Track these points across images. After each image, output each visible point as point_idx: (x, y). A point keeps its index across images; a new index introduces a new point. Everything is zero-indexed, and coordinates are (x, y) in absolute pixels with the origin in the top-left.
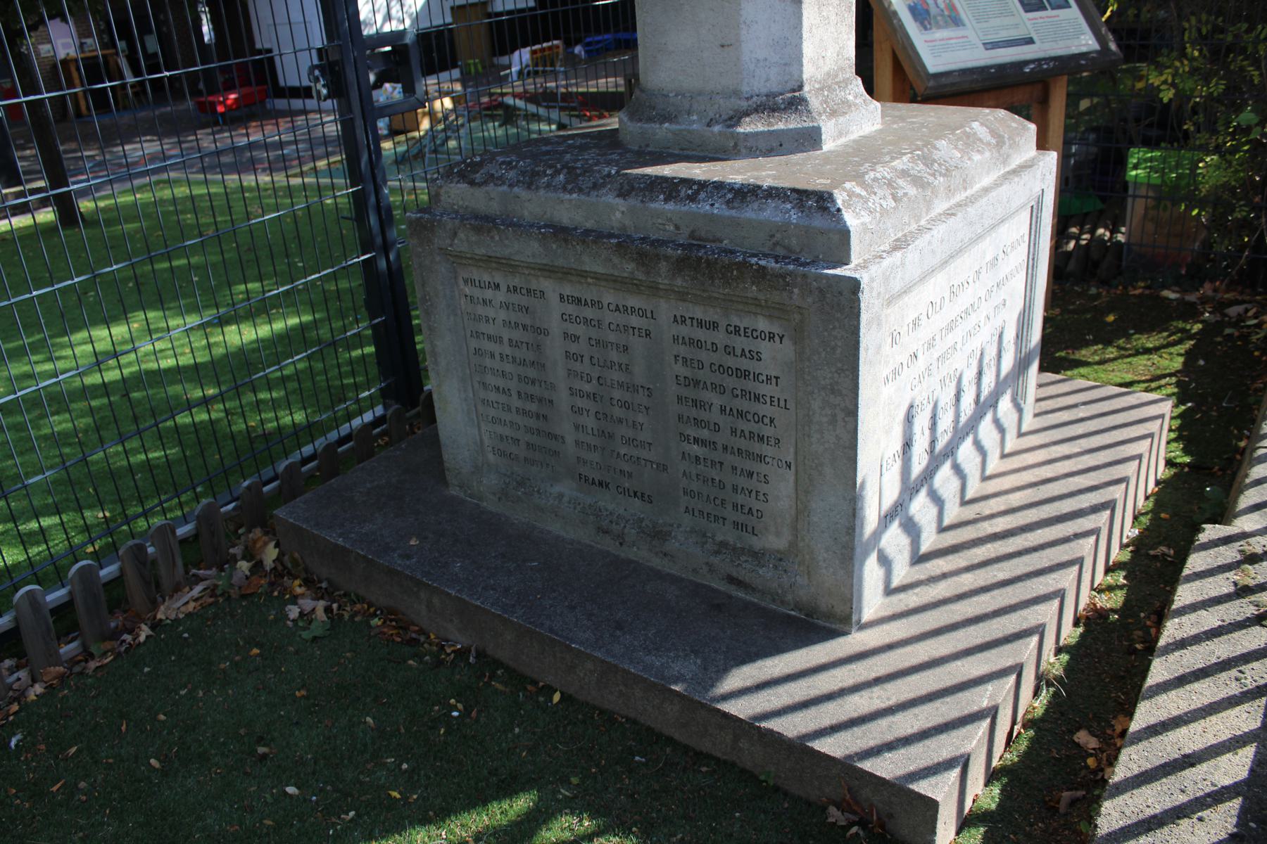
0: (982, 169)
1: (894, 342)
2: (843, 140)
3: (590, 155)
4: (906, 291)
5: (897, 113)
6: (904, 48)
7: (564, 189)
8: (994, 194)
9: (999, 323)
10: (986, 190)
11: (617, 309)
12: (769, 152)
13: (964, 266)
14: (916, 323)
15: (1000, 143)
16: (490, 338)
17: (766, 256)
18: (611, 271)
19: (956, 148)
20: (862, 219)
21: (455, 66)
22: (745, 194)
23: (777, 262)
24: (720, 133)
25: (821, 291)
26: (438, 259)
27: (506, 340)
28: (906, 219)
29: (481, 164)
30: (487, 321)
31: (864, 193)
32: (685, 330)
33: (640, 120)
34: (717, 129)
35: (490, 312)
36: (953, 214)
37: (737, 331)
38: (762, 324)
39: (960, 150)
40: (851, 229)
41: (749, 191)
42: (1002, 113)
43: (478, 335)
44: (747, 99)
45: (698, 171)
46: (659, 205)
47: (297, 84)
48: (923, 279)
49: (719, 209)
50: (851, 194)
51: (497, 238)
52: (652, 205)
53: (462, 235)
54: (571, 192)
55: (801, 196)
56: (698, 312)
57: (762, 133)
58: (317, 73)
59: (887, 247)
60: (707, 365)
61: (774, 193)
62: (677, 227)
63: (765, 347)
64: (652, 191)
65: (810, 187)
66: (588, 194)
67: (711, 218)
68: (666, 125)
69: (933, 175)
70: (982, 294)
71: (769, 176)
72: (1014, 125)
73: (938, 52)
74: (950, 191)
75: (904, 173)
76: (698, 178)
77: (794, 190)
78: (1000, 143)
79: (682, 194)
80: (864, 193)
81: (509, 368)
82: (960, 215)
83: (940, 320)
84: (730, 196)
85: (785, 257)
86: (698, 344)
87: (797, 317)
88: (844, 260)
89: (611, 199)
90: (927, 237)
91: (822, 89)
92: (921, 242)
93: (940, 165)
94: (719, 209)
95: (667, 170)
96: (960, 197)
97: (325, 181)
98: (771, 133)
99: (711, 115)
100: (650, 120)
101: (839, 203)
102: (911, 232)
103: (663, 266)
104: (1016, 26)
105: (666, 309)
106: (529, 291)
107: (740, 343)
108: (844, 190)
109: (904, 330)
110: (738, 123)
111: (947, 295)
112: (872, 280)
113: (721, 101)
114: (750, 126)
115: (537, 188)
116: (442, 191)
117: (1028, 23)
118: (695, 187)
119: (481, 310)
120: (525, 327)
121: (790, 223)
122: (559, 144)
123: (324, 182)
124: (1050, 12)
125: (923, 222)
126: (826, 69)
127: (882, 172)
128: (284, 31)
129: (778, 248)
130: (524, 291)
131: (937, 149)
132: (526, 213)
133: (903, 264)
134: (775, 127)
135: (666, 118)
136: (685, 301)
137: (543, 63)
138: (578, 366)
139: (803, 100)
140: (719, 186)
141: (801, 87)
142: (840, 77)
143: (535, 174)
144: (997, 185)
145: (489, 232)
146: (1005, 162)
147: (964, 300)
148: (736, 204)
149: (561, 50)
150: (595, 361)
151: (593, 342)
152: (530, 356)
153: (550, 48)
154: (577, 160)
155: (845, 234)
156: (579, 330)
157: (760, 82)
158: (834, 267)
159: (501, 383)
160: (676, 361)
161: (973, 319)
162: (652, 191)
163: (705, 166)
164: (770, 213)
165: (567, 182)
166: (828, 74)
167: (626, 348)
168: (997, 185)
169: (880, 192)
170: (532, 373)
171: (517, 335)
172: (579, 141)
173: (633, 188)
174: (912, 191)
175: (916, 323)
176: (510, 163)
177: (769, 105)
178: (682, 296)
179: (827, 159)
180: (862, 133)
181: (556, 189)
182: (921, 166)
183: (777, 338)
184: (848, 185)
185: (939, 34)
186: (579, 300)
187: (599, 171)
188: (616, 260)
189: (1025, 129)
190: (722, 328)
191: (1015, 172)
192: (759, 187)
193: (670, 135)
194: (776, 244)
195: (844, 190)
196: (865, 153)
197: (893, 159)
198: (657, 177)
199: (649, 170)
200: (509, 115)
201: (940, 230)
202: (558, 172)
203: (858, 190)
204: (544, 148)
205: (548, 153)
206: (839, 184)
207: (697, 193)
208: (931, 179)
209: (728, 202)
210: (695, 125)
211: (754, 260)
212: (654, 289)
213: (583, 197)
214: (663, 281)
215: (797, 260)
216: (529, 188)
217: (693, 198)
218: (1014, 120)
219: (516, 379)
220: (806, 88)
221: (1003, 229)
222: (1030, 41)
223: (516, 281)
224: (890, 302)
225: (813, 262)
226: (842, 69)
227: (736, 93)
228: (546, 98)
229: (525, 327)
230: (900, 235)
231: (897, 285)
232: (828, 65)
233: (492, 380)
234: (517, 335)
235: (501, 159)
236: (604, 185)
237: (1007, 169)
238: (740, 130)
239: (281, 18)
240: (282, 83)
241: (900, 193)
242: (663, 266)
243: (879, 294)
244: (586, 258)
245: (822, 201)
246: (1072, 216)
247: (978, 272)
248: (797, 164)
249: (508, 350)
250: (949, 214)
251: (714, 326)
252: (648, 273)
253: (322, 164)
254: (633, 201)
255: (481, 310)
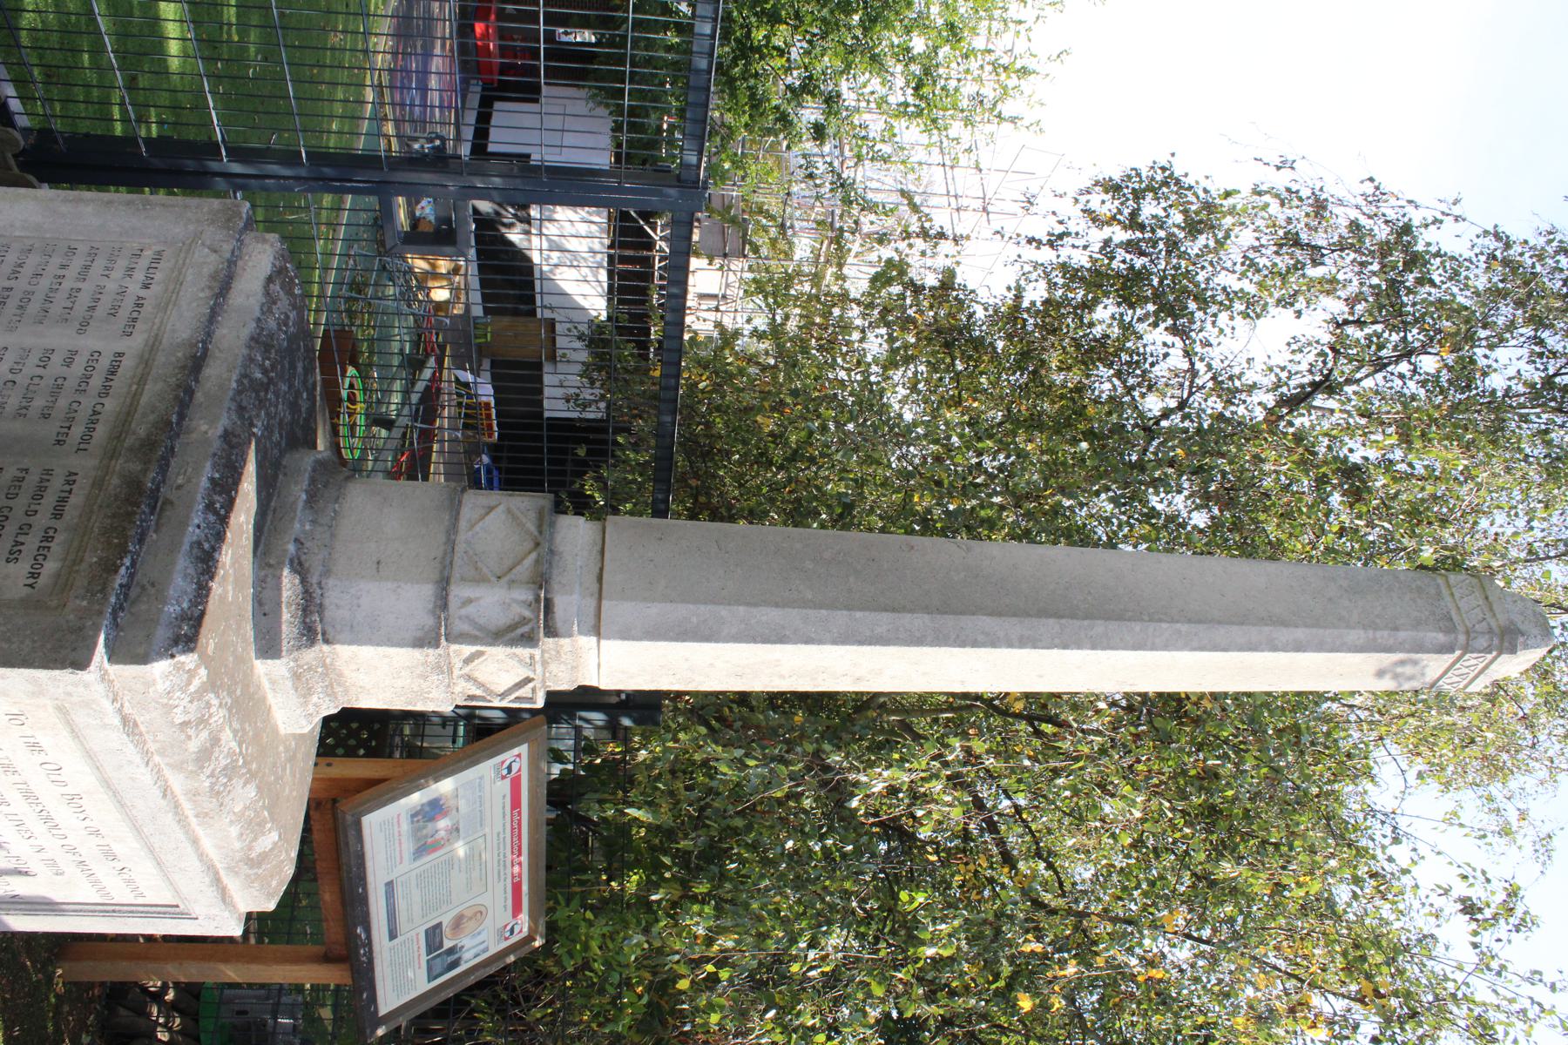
0: (221, 838)
1: (14, 716)
2: (266, 685)
3: (282, 410)
4: (75, 733)
5: (300, 756)
6: (393, 790)
7: (245, 376)
8: (189, 849)
9: (34, 865)
10: (195, 842)
11: (95, 413)
12: (258, 601)
13: (103, 812)
14: (35, 747)
15: (253, 863)
16: (87, 267)
17: (132, 576)
18: (140, 410)
19: (246, 808)
20: (160, 681)
21: (487, 311)
22: (206, 562)
23: (121, 586)
24: (286, 551)
25: (80, 629)
26: (191, 227)
27: (80, 285)
28: (160, 737)
29: (290, 293)
30: (107, 269)
31: (192, 688)
32: (57, 483)
33: (314, 470)
34: (291, 548)
35: (117, 274)
36: (165, 796)
37: (48, 539)
38: (50, 567)
39: (242, 813)
40: (148, 667)
41: (209, 567)
42: (289, 871)
43: (93, 254)
44: (319, 583)
45: (242, 518)
46: (207, 471)
47: (493, 122)
48: (89, 755)
49: (192, 533)
50: (191, 674)
51: (201, 295)
52: (208, 465)
53: (213, 257)
54: (239, 382)
55: (197, 621)
56: (76, 500)
57: (280, 595)
58: (438, 143)
59: (127, 709)
60: (11, 503)
61: (202, 592)
62: (179, 487)
63: (23, 567)
64: (226, 466)
65: (204, 631)
66: (232, 399)
67: (184, 524)
68: (304, 496)
69: (212, 775)
70: (71, 841)
71: (225, 592)
72: (274, 883)
73: (385, 831)
74: (194, 794)
75: (215, 741)
76: (233, 516)
77: (203, 613)
78: (253, 863)
79: (216, 497)
80: (192, 688)
81: (45, 283)
82: (164, 803)
83: (40, 783)
84: (206, 546)
85: (126, 596)
86: (38, 495)
87: (54, 603)
88: (114, 656)
89: (223, 422)
90: (137, 759)
91: (324, 665)
92: (131, 751)
93: (225, 785)
94: (192, 533)
95: (248, 487)
96: (187, 807)
97: (365, 126)
98: (279, 604)
99: (308, 544)
100: (313, 481)
101: (181, 658)
102: (145, 742)
103: (136, 467)
104: (410, 920)
105: (85, 466)
106: (135, 320)
107: (32, 542)
108: (198, 667)
109: (27, 730)
110: (294, 570)
111: (69, 790)
112: (86, 686)
113: (320, 557)
114: (289, 583)
115: (250, 347)
116: (267, 247)
117: (413, 933)
118: (222, 512)
119: (122, 263)
120: (92, 308)
121: (165, 603)
122: (305, 382)
123: (369, 122)
124: (424, 958)
125: (157, 759)
126: (346, 673)
127: (218, 716)
128: (556, 122)
129: (138, 590)
130: (135, 315)
131: (245, 785)
132: (225, 331)
133: (105, 726)
134: (284, 610)
135: (312, 498)
136: (93, 485)
137: (471, 416)
138: (33, 359)
139: (312, 642)
140: (220, 537)
141: (327, 641)
142: (338, 689)
143: (267, 348)
144: (201, 856)
145: (210, 288)
146: (229, 869)
147: (64, 815)
148: (195, 550)
149: (486, 439)
150: (36, 380)
151: (60, 382)
152: (56, 309)
153: (490, 427)
154: (277, 394)
155: (143, 659)
156: (78, 368)
157: (338, 599)
158: (106, 645)
159: (28, 270)
160: (22, 470)
161: (39, 828)
162: (226, 466)
163: (249, 528)
164: (180, 583)
165: (251, 380)
166: (341, 675)
167: (45, 416)
168: (201, 856)
169: (193, 707)
170: (34, 307)
171: (84, 300)
172: (304, 406)
173: (232, 447)
174: (193, 746)
175: (35, 747)
176: (286, 325)
177: (310, 606)
178: (99, 483)
179: (241, 660)
180: (274, 708)
181: (245, 366)
182: (224, 762)
183: (31, 581)
184: (203, 672)
185: (405, 826)
186: (113, 373)
187: (258, 416)
188: (152, 417)
189: (270, 896)
190: (53, 523)
191: (217, 881)
192: (212, 578)
193: (292, 499)
194: (143, 588)
195: (198, 667)
196: (249, 709)
197: (235, 732)
198: (241, 474)
199: (251, 468)
200: (414, 364)
201: (146, 777)
202: (265, 372)
203: (196, 683)
204: (300, 366)
205: (293, 366)
206: (205, 660)
207: (216, 513)
208: (208, 772)
209: (199, 543)
210: (300, 524)
211: (127, 561)
212: (111, 454)
213: (231, 393)
214: (118, 464)
215: (122, 608)
216: (252, 338)
217: (210, 507)
218: (280, 884)
219: (30, 288)
220: (326, 648)
221: (149, 866)
222: (393, 935)
223: (148, 308)
224: (61, 709)
225: (115, 625)
226: (346, 691)
227: (327, 573)
228: (429, 405)
229: (92, 308)
230: (142, 728)
231: (80, 718)
232: (350, 675)
233: (32, 261)
234: (84, 300)
235: (293, 315)
236: (241, 417)
237: (222, 873)
238: (286, 572)
239: (571, 123)
240: (498, 105)
241: (191, 732)
242: (136, 467)
243: (70, 694)
244: (160, 385)
245: (186, 636)
246: (197, 1021)
247: (97, 833)
248: (239, 628)
249: (67, 284)
250: (166, 792)
251: (58, 514)
252: (131, 449)
253: (390, 128)
254: (217, 444)
255: (122, 263)
